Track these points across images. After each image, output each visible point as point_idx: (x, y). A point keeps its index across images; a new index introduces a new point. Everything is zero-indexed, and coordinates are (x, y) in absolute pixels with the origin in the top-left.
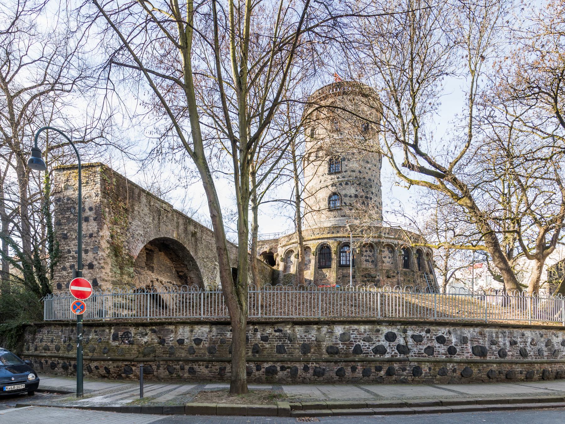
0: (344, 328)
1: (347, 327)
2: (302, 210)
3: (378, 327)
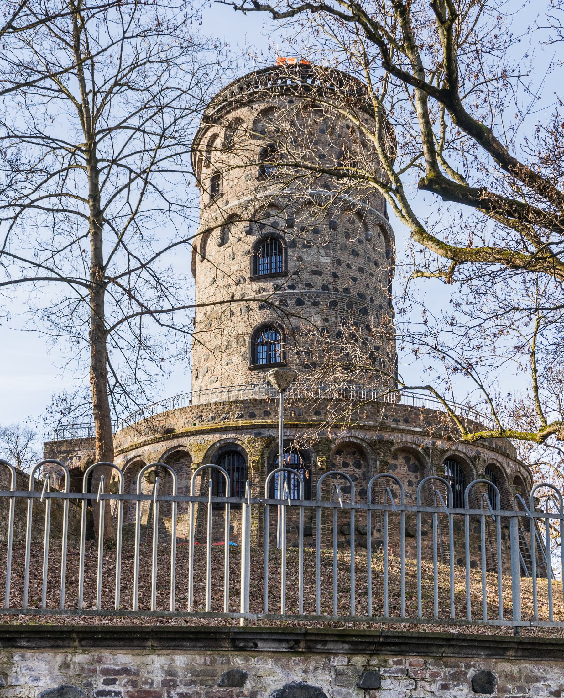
0: (65, 665)
1: (79, 658)
2: (109, 307)
3: (238, 662)
